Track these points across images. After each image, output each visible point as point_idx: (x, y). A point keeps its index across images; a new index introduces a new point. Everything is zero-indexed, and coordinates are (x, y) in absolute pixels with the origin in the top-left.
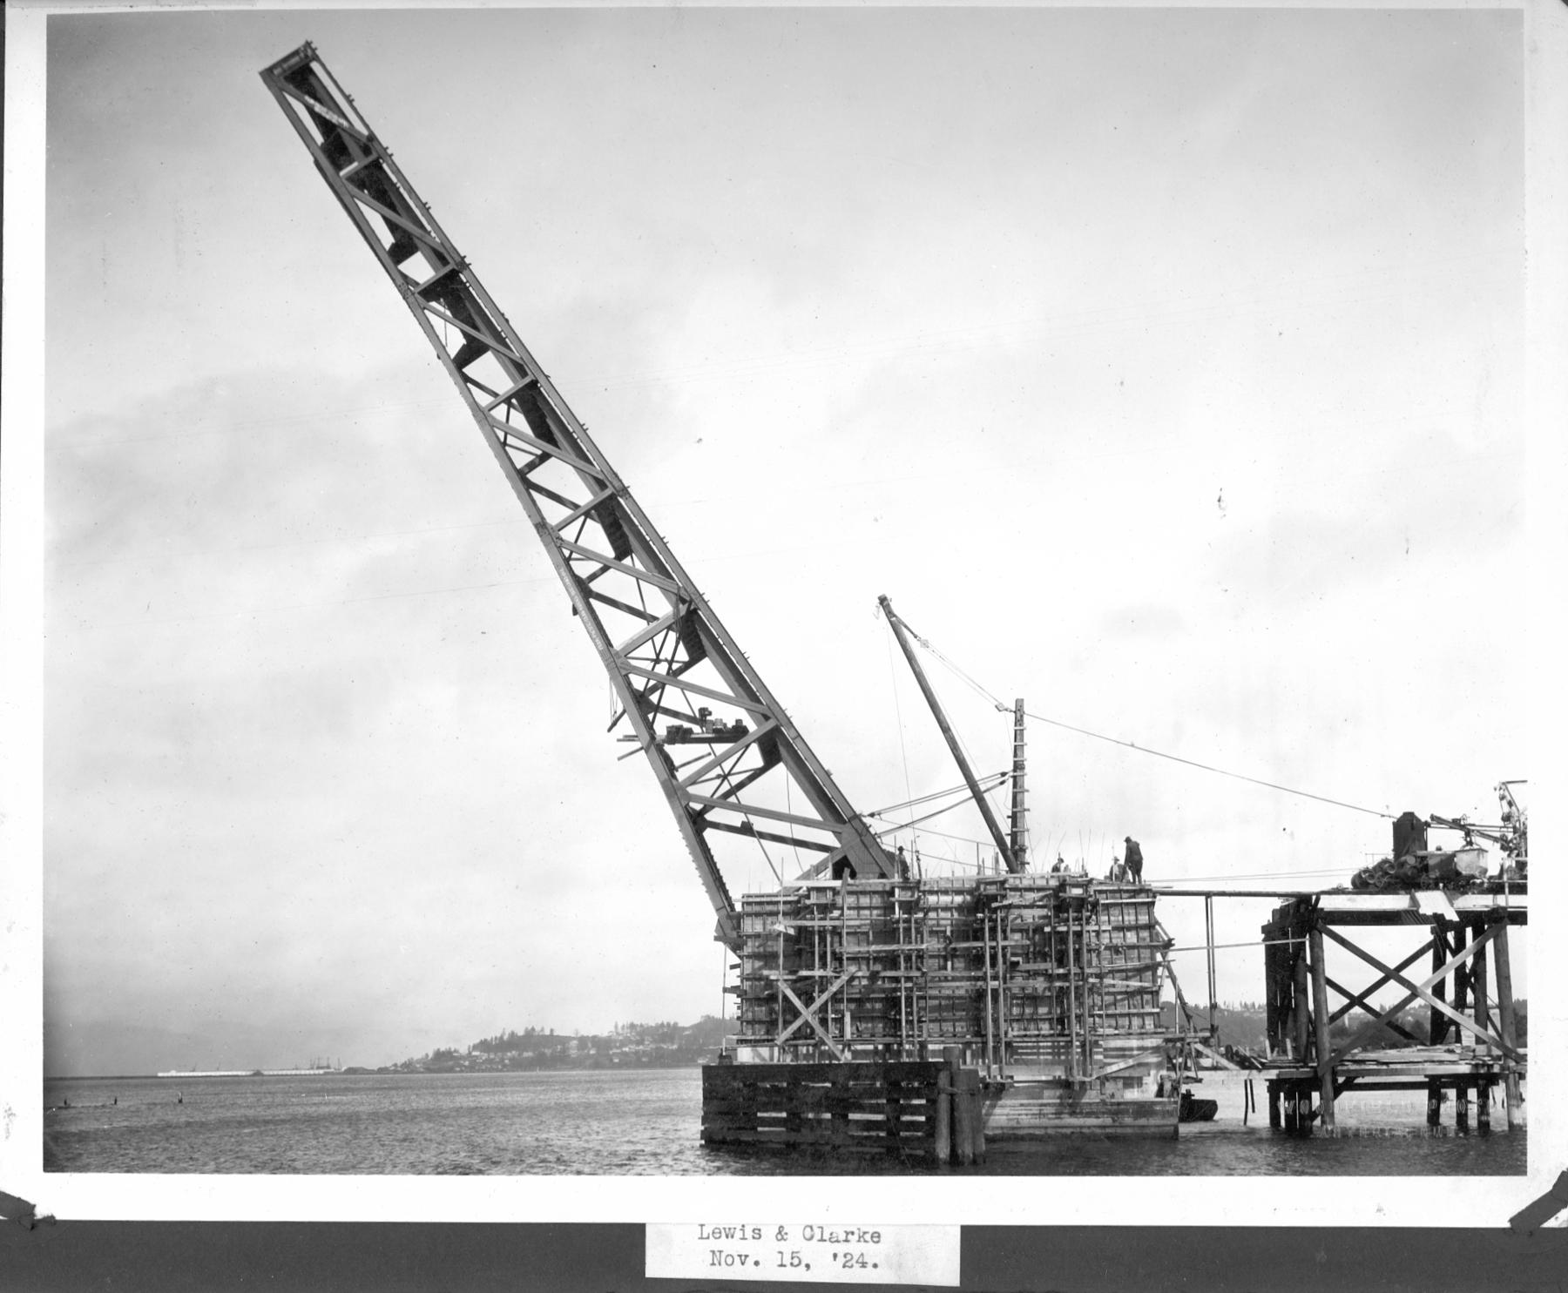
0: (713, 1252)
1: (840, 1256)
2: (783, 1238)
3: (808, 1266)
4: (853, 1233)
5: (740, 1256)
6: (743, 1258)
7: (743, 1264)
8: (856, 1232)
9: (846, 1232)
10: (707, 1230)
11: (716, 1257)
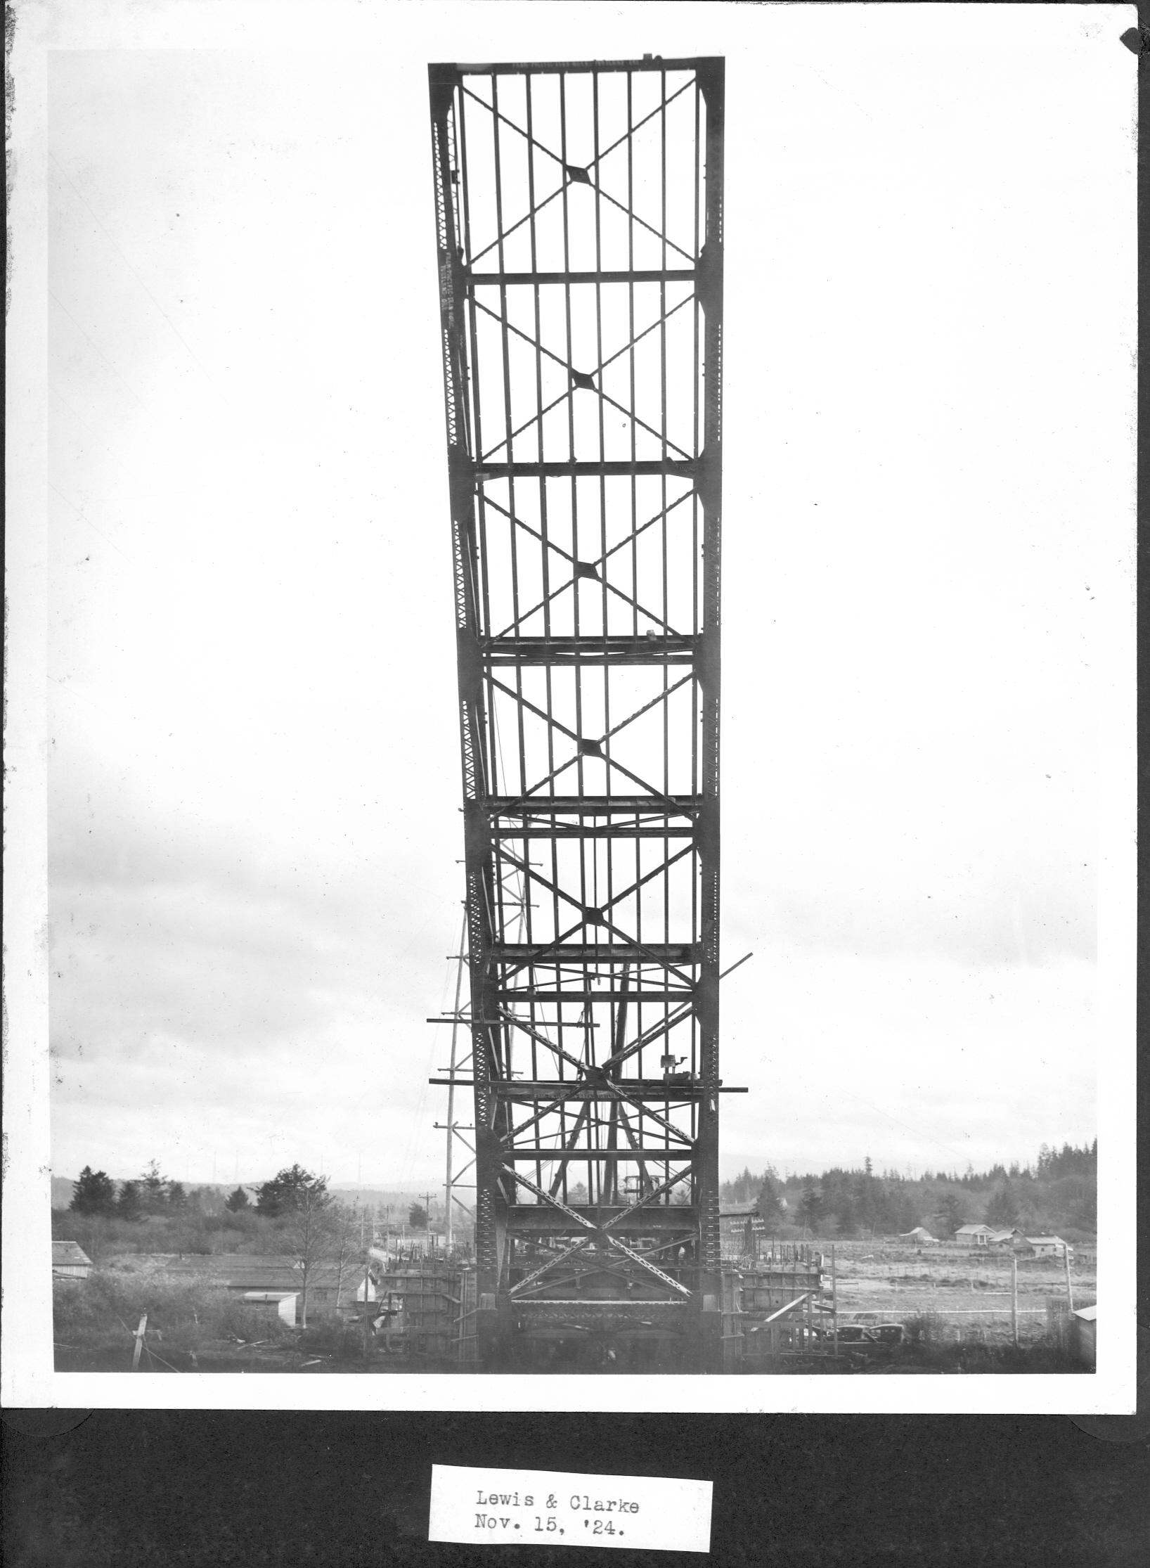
0: (478, 1515)
2: (552, 1506)
3: (562, 1531)
5: (502, 1519)
6: (505, 1521)
7: (504, 1526)
8: (618, 1503)
9: (609, 1502)
10: (485, 1496)
11: (481, 1520)
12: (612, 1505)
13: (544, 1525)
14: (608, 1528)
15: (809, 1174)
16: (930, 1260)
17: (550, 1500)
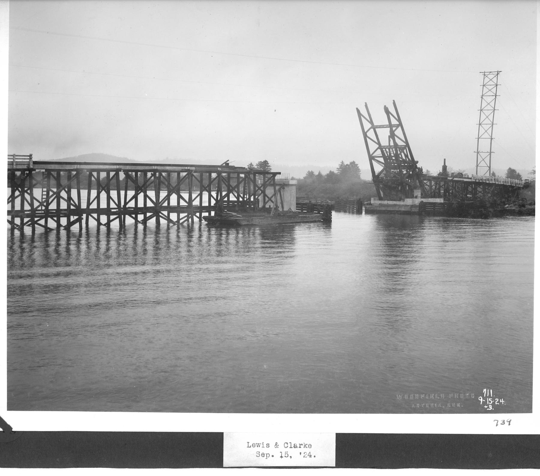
1: (302, 454)
3: (291, 457)
4: (302, 445)
10: (250, 444)
12: (301, 445)
13: (283, 455)
14: (309, 455)
15: (332, 171)
16: (233, 271)
17: (276, 445)
